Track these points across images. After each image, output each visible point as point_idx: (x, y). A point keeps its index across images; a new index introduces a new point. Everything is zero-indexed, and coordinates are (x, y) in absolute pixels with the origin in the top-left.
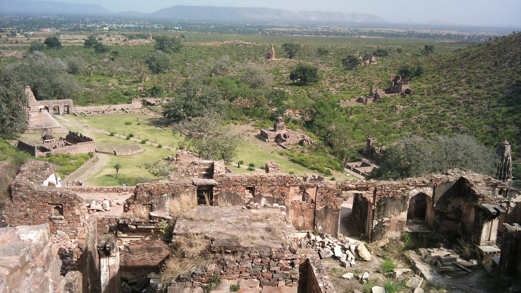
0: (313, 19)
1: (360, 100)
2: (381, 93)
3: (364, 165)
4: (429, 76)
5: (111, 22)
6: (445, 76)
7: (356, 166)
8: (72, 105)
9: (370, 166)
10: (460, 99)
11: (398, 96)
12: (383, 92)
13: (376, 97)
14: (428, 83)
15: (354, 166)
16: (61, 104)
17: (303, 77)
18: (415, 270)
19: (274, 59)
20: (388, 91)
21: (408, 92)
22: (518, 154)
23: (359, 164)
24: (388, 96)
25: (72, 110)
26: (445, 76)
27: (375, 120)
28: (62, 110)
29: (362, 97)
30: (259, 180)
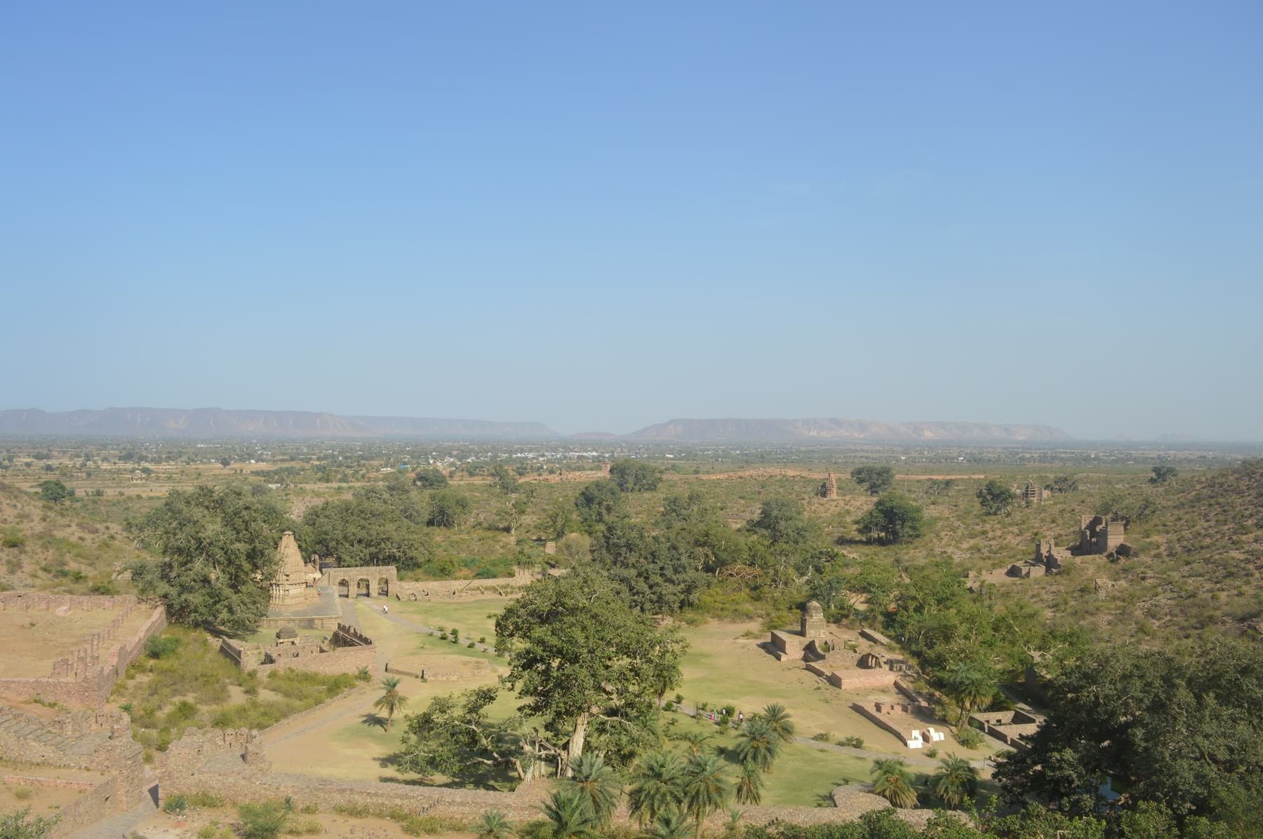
0: (928, 434)
1: (1013, 572)
2: (1061, 554)
3: (1019, 719)
4: (1169, 518)
5: (555, 449)
6: (1206, 515)
7: (999, 721)
8: (395, 578)
9: (1033, 721)
10: (1248, 561)
11: (1100, 559)
12: (1068, 554)
13: (1050, 563)
14: (1168, 532)
15: (993, 722)
16: (374, 574)
17: (891, 524)
18: (875, 641)
19: (834, 496)
20: (1076, 551)
21: (1123, 551)
22: (1063, 837)
23: (1007, 716)
24: (1078, 559)
25: (395, 587)
26: (1206, 515)
27: (1048, 614)
28: (374, 588)
29: (1019, 564)
30: (519, 644)
